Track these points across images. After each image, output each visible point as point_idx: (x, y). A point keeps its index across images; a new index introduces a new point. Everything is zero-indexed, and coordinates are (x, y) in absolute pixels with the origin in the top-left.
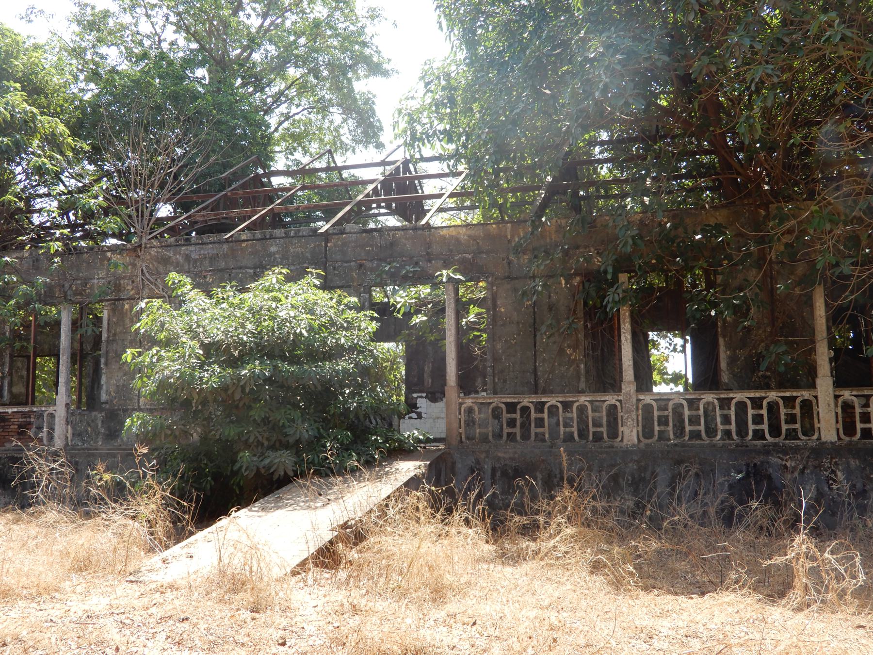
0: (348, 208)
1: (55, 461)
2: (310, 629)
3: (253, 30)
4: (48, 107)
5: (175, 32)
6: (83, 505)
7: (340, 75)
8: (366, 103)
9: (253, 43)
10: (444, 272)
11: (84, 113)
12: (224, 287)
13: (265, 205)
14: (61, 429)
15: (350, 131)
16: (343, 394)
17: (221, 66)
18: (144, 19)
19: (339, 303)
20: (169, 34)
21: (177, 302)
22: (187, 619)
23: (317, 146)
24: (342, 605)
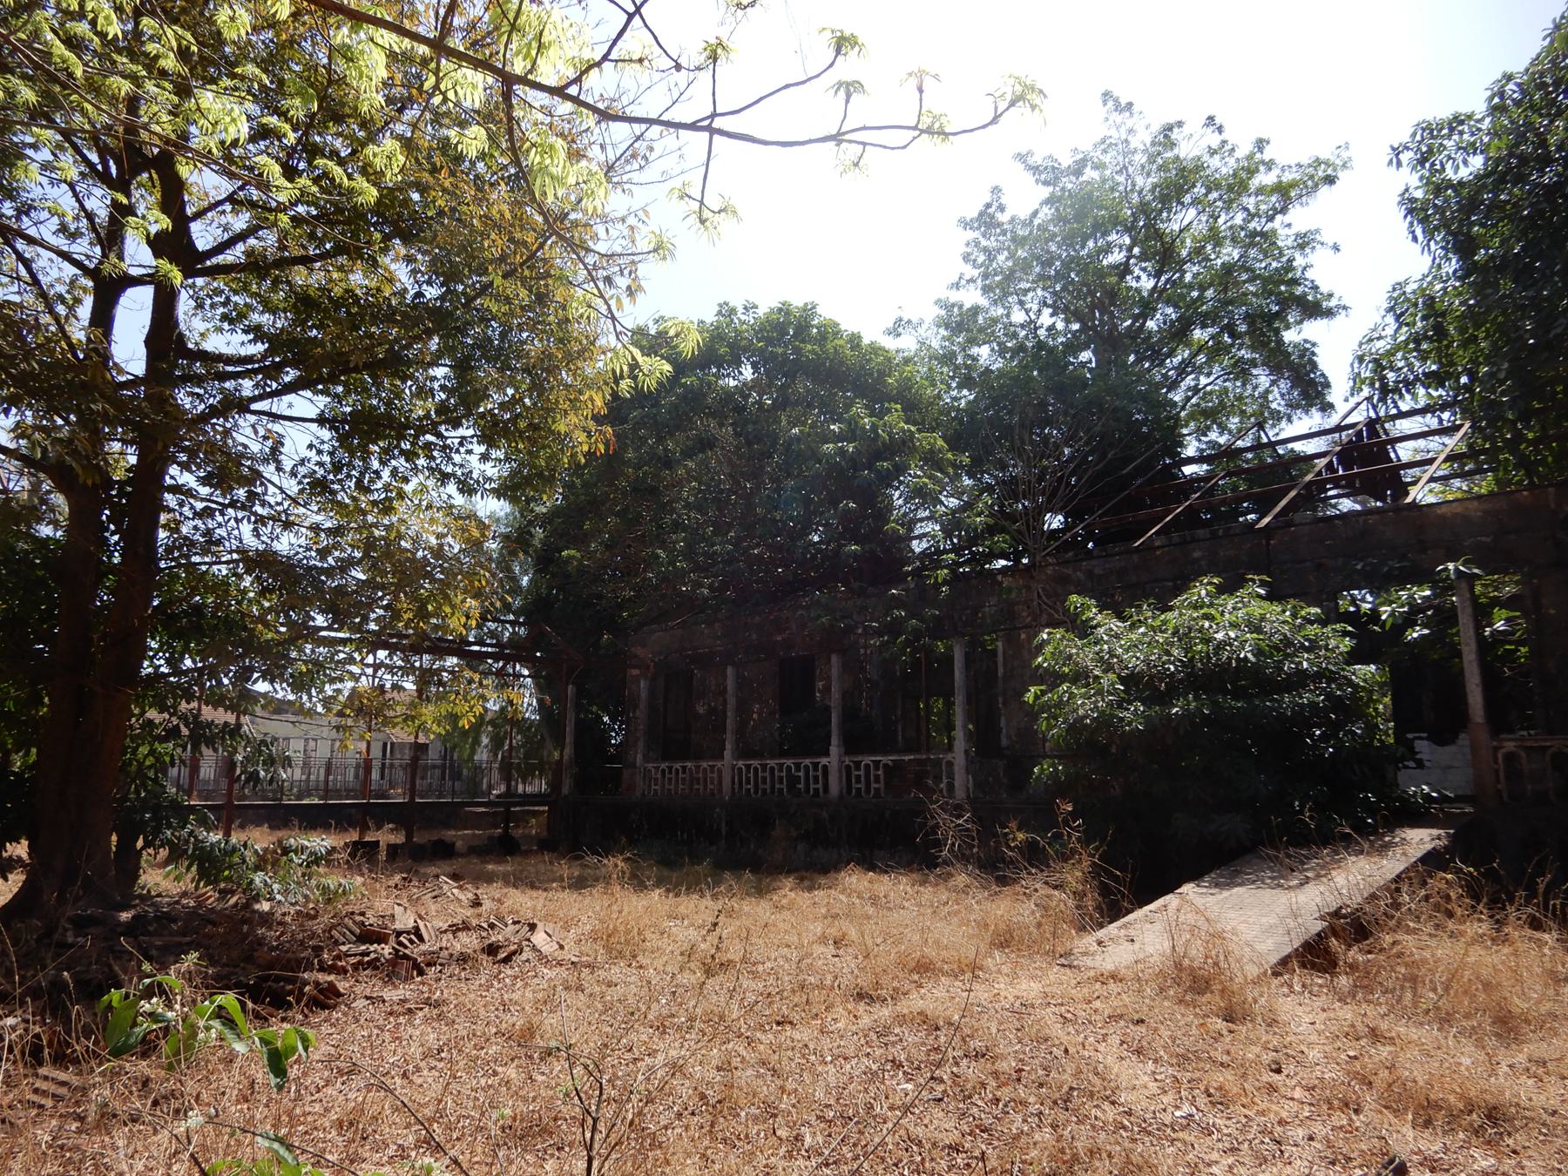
0: (1293, 493)
1: (958, 817)
2: (1314, 1054)
3: (1145, 294)
4: (923, 423)
5: (1052, 315)
6: (997, 869)
7: (1264, 330)
8: (1302, 356)
9: (1147, 307)
10: (1451, 566)
11: (961, 422)
12: (1140, 606)
13: (1180, 503)
14: (960, 779)
15: (1282, 395)
16: (1311, 736)
17: (1110, 344)
18: (1016, 308)
19: (1294, 616)
20: (1046, 319)
21: (1084, 630)
22: (1142, 1021)
23: (1236, 420)
24: (1353, 1026)
